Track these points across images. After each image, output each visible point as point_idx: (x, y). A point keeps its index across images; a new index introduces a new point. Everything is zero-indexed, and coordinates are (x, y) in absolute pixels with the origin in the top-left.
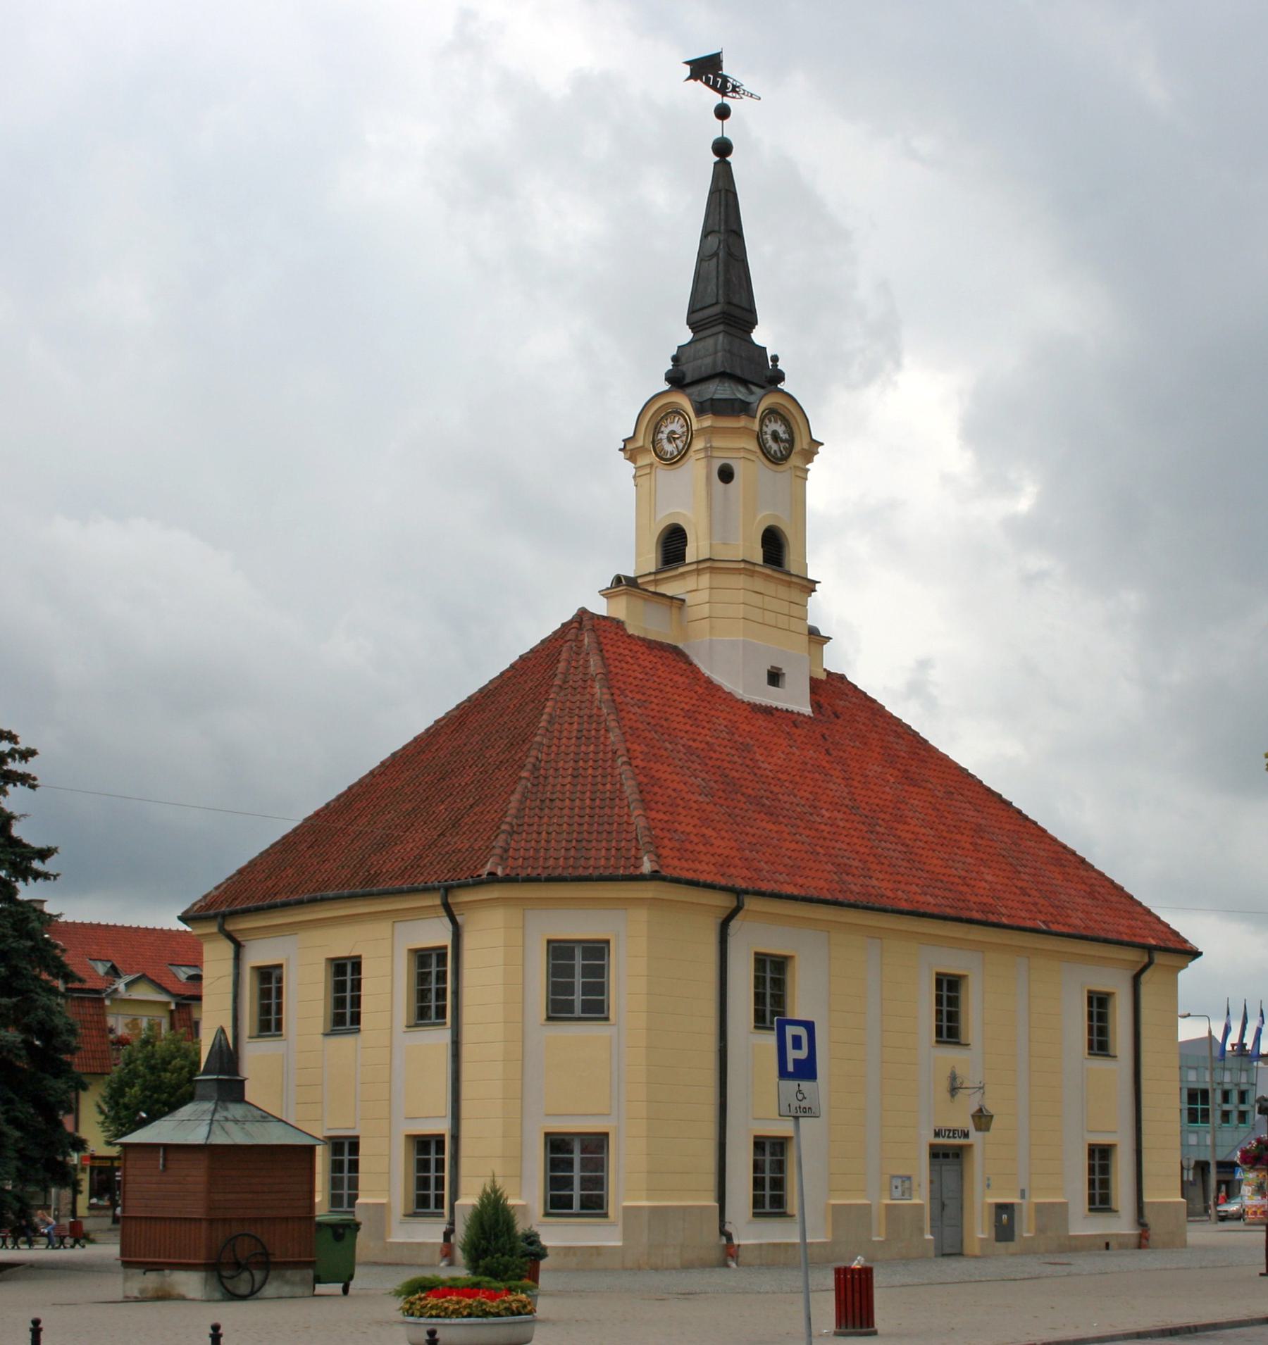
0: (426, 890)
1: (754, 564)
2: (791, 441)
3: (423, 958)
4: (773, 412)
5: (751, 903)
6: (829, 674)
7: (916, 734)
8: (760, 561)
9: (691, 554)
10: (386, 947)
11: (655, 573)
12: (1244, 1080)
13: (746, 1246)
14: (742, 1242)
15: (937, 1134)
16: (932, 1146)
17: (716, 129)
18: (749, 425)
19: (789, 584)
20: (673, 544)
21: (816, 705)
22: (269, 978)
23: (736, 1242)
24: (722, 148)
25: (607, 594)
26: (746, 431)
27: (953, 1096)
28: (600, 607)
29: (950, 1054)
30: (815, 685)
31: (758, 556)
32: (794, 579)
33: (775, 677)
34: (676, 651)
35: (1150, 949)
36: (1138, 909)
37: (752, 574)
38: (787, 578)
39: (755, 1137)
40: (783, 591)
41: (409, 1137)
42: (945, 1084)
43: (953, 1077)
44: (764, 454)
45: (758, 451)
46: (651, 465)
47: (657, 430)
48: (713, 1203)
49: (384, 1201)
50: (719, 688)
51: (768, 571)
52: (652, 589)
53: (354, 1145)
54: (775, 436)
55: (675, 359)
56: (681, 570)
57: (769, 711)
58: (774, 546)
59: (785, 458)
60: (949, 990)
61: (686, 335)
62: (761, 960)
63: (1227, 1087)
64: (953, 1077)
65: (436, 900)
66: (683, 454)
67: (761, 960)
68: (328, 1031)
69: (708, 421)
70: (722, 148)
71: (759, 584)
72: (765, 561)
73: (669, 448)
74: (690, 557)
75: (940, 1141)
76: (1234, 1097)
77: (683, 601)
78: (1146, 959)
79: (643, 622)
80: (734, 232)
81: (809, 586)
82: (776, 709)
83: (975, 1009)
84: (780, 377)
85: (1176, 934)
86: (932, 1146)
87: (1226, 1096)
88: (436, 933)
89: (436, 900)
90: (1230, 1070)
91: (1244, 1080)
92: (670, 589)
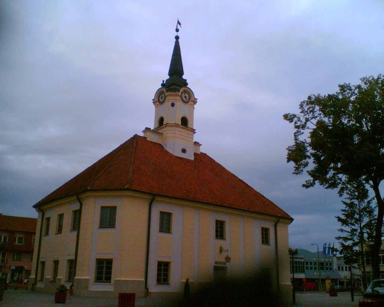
0: (72, 195)
1: (179, 125)
2: (190, 98)
3: (75, 212)
4: (185, 92)
5: (157, 198)
6: (201, 153)
7: (222, 167)
8: (181, 124)
9: (164, 123)
10: (67, 210)
11: (157, 128)
12: (330, 260)
13: (153, 292)
14: (152, 291)
15: (216, 263)
16: (214, 267)
17: (176, 34)
18: (179, 94)
19: (188, 130)
20: (161, 121)
21: (195, 159)
22: (48, 219)
23: (150, 291)
24: (177, 38)
25: (144, 132)
26: (178, 95)
27: (221, 253)
28: (142, 134)
29: (220, 242)
30: (195, 154)
31: (180, 123)
32: (189, 129)
33: (184, 151)
34: (160, 145)
35: (278, 217)
36: (277, 208)
37: (178, 127)
38: (188, 128)
39: (158, 261)
40: (186, 131)
41: (68, 260)
42: (218, 250)
43: (221, 248)
44: (182, 101)
45: (181, 100)
46: (158, 105)
47: (159, 97)
48: (144, 280)
49: (88, 278)
50: (169, 153)
51: (182, 126)
52: (157, 131)
53: (109, 262)
54: (185, 97)
55: (194, 108)
56: (162, 126)
57: (181, 158)
58: (185, 122)
59: (188, 102)
60: (220, 225)
61: (168, 77)
62: (162, 213)
63: (327, 262)
64: (221, 248)
65: (75, 198)
66: (164, 101)
67: (162, 213)
68: (57, 233)
69: (169, 93)
70: (177, 38)
71: (180, 129)
72: (181, 124)
73: (161, 100)
74: (164, 124)
75: (216, 265)
76: (329, 264)
77: (163, 134)
78: (278, 220)
79: (152, 138)
80: (179, 55)
81: (193, 131)
82: (184, 158)
83: (228, 230)
84: (187, 84)
85: (287, 214)
86: (214, 267)
87: (327, 264)
88: (77, 206)
89: (75, 198)
90: (327, 258)
91: (330, 260)
92: (160, 131)
